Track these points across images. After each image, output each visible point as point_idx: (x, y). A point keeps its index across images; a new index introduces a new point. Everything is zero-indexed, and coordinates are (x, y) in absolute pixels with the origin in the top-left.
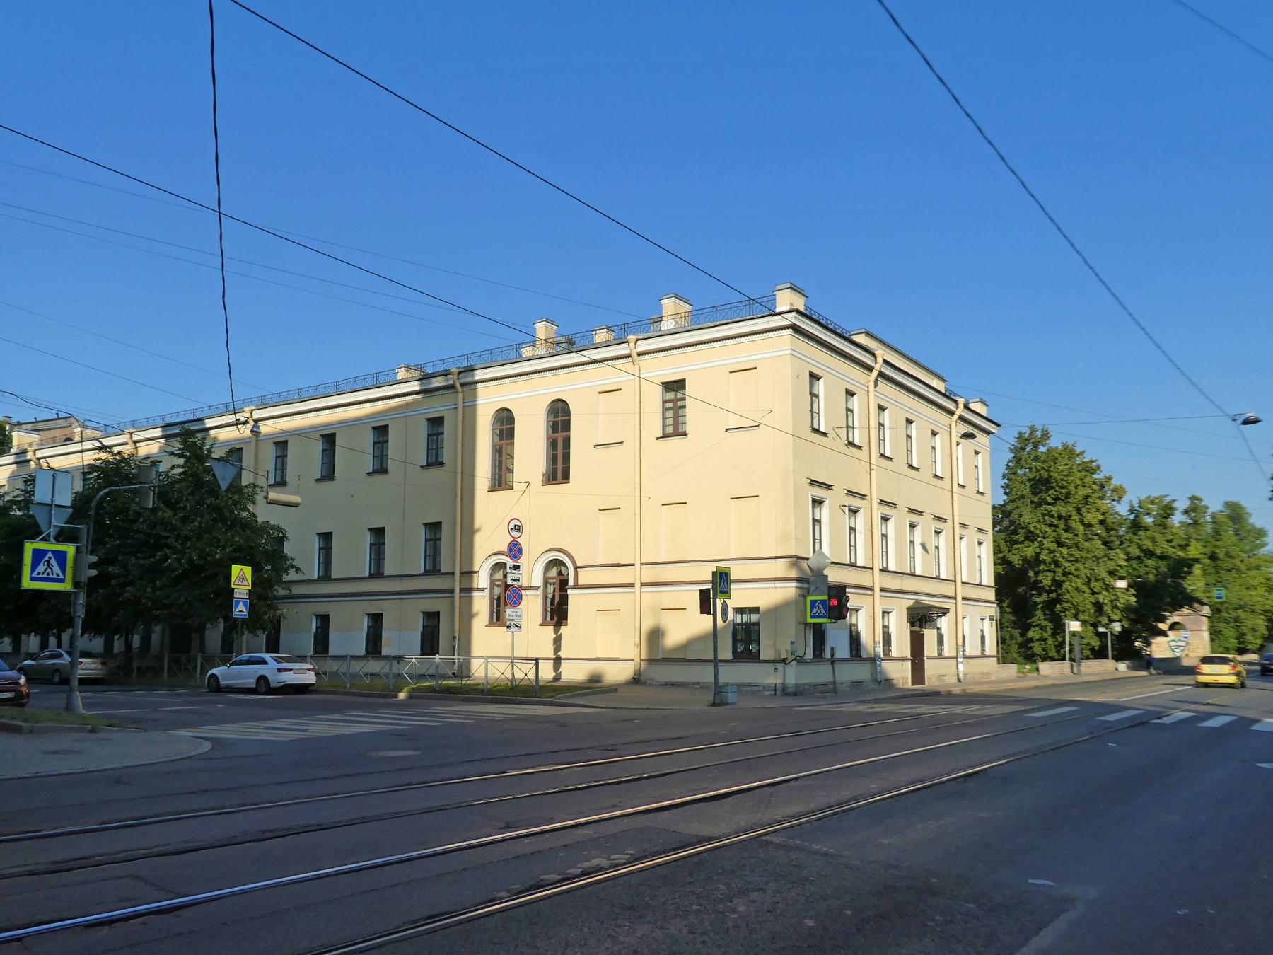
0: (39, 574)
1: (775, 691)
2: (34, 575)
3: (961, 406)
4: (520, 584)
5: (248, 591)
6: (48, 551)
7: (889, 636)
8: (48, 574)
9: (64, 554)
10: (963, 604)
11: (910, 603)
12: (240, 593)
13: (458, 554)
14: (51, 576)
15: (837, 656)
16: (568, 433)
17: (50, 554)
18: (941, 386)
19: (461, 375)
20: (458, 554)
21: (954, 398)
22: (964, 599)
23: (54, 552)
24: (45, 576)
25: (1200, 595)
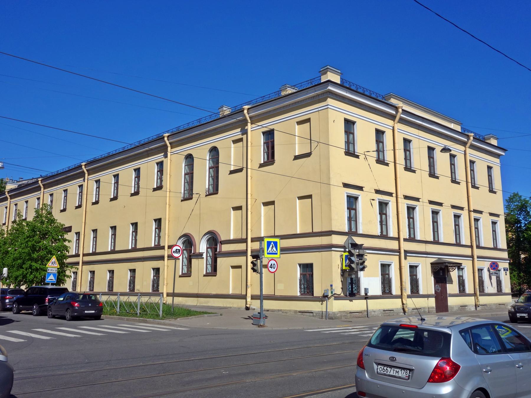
0: (269, 251)
1: (322, 316)
2: (268, 252)
3: (472, 138)
4: (69, 250)
5: (57, 269)
6: (271, 242)
7: (463, 281)
8: (272, 251)
9: (276, 242)
10: (477, 260)
11: (433, 260)
12: (51, 270)
13: (167, 235)
14: (273, 252)
15: (370, 294)
16: (218, 165)
17: (272, 243)
18: (458, 128)
19: (169, 137)
20: (167, 235)
21: (467, 133)
22: (478, 257)
23: (274, 242)
24: (271, 252)
25: (19, 249)
